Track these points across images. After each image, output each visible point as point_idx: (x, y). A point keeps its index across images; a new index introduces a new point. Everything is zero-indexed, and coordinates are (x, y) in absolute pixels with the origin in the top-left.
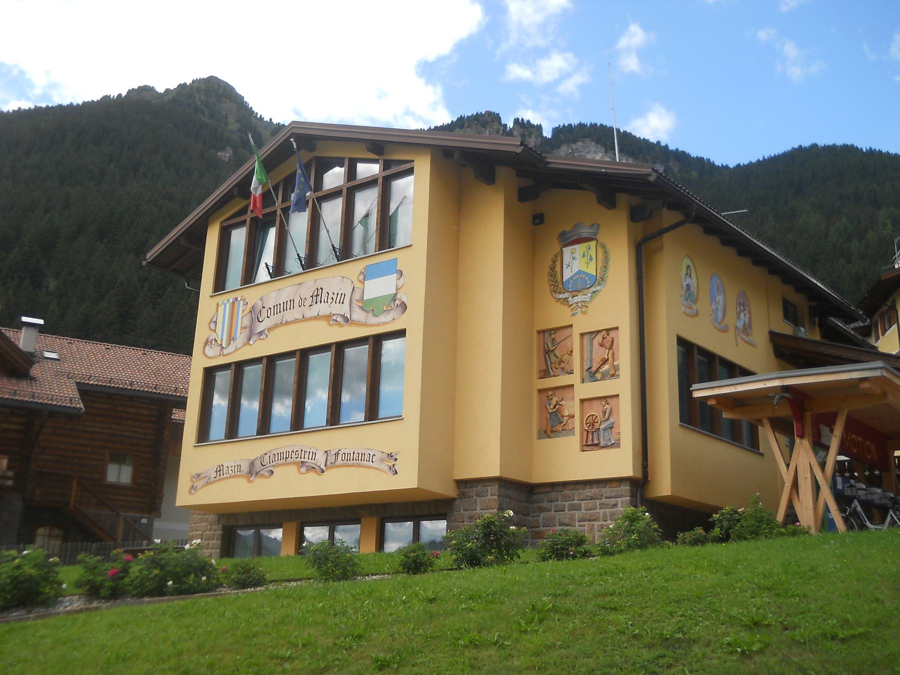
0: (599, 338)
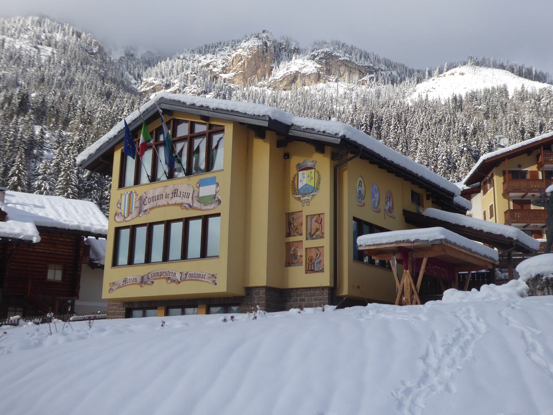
0: (315, 218)
